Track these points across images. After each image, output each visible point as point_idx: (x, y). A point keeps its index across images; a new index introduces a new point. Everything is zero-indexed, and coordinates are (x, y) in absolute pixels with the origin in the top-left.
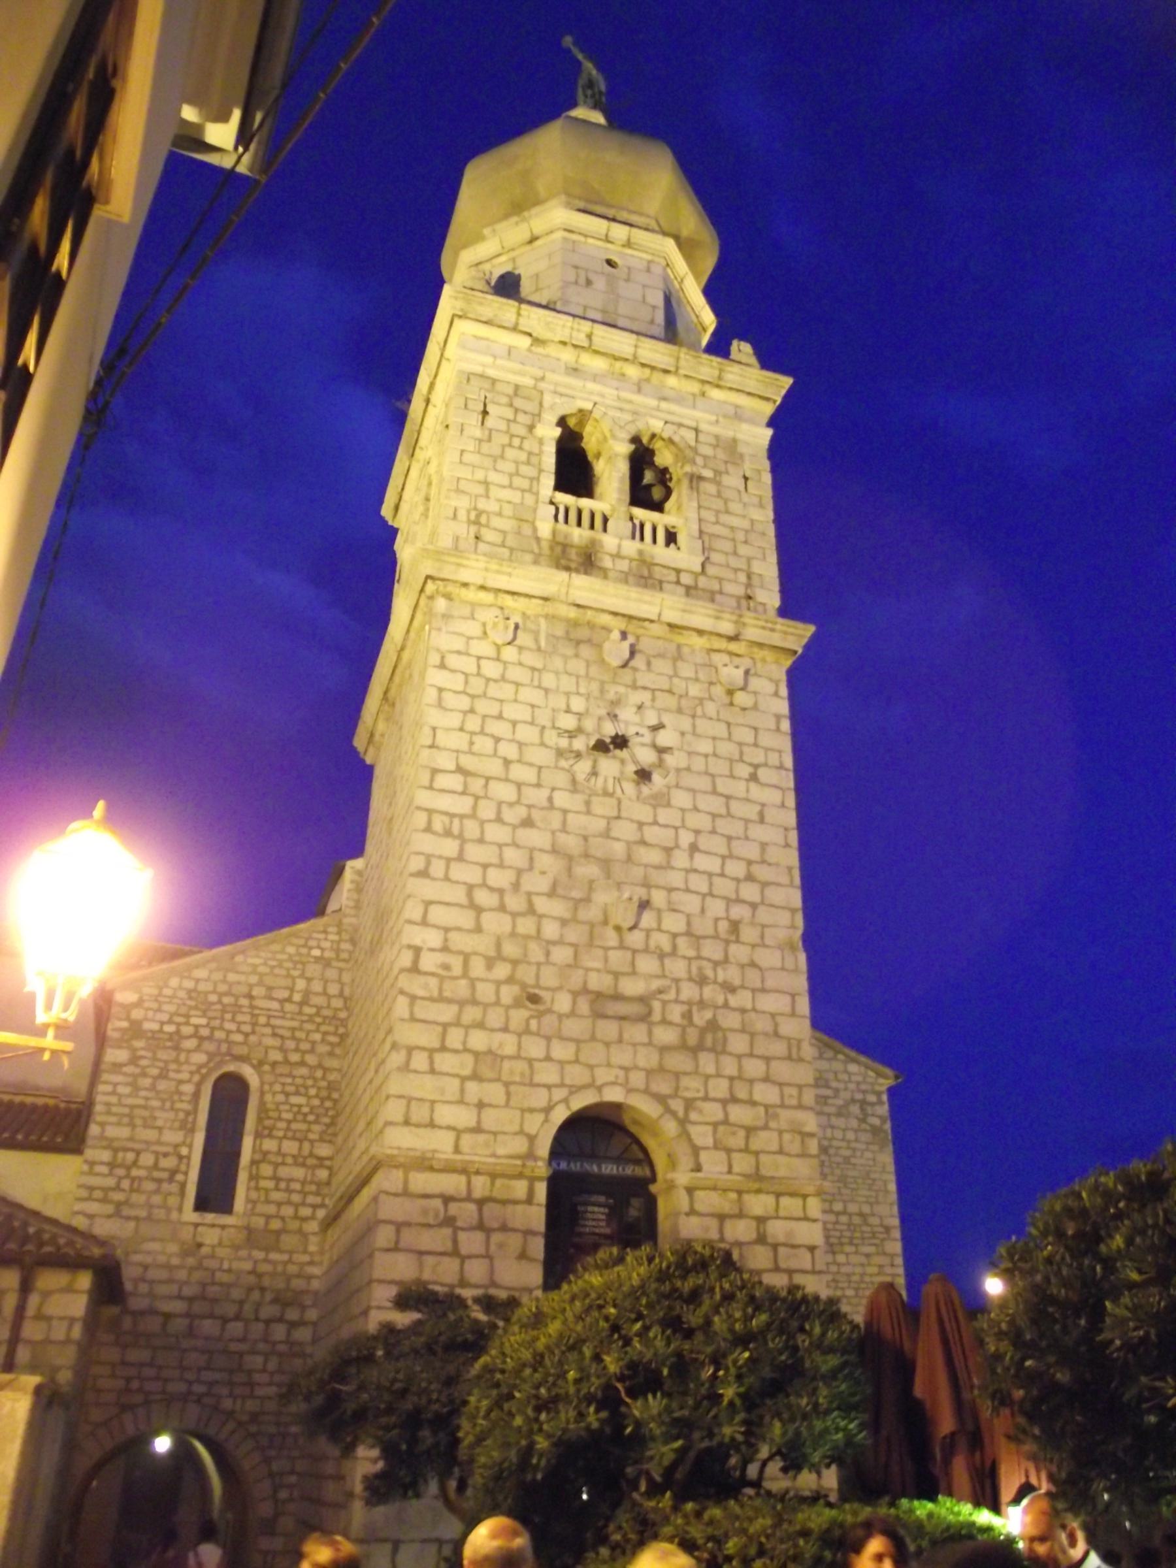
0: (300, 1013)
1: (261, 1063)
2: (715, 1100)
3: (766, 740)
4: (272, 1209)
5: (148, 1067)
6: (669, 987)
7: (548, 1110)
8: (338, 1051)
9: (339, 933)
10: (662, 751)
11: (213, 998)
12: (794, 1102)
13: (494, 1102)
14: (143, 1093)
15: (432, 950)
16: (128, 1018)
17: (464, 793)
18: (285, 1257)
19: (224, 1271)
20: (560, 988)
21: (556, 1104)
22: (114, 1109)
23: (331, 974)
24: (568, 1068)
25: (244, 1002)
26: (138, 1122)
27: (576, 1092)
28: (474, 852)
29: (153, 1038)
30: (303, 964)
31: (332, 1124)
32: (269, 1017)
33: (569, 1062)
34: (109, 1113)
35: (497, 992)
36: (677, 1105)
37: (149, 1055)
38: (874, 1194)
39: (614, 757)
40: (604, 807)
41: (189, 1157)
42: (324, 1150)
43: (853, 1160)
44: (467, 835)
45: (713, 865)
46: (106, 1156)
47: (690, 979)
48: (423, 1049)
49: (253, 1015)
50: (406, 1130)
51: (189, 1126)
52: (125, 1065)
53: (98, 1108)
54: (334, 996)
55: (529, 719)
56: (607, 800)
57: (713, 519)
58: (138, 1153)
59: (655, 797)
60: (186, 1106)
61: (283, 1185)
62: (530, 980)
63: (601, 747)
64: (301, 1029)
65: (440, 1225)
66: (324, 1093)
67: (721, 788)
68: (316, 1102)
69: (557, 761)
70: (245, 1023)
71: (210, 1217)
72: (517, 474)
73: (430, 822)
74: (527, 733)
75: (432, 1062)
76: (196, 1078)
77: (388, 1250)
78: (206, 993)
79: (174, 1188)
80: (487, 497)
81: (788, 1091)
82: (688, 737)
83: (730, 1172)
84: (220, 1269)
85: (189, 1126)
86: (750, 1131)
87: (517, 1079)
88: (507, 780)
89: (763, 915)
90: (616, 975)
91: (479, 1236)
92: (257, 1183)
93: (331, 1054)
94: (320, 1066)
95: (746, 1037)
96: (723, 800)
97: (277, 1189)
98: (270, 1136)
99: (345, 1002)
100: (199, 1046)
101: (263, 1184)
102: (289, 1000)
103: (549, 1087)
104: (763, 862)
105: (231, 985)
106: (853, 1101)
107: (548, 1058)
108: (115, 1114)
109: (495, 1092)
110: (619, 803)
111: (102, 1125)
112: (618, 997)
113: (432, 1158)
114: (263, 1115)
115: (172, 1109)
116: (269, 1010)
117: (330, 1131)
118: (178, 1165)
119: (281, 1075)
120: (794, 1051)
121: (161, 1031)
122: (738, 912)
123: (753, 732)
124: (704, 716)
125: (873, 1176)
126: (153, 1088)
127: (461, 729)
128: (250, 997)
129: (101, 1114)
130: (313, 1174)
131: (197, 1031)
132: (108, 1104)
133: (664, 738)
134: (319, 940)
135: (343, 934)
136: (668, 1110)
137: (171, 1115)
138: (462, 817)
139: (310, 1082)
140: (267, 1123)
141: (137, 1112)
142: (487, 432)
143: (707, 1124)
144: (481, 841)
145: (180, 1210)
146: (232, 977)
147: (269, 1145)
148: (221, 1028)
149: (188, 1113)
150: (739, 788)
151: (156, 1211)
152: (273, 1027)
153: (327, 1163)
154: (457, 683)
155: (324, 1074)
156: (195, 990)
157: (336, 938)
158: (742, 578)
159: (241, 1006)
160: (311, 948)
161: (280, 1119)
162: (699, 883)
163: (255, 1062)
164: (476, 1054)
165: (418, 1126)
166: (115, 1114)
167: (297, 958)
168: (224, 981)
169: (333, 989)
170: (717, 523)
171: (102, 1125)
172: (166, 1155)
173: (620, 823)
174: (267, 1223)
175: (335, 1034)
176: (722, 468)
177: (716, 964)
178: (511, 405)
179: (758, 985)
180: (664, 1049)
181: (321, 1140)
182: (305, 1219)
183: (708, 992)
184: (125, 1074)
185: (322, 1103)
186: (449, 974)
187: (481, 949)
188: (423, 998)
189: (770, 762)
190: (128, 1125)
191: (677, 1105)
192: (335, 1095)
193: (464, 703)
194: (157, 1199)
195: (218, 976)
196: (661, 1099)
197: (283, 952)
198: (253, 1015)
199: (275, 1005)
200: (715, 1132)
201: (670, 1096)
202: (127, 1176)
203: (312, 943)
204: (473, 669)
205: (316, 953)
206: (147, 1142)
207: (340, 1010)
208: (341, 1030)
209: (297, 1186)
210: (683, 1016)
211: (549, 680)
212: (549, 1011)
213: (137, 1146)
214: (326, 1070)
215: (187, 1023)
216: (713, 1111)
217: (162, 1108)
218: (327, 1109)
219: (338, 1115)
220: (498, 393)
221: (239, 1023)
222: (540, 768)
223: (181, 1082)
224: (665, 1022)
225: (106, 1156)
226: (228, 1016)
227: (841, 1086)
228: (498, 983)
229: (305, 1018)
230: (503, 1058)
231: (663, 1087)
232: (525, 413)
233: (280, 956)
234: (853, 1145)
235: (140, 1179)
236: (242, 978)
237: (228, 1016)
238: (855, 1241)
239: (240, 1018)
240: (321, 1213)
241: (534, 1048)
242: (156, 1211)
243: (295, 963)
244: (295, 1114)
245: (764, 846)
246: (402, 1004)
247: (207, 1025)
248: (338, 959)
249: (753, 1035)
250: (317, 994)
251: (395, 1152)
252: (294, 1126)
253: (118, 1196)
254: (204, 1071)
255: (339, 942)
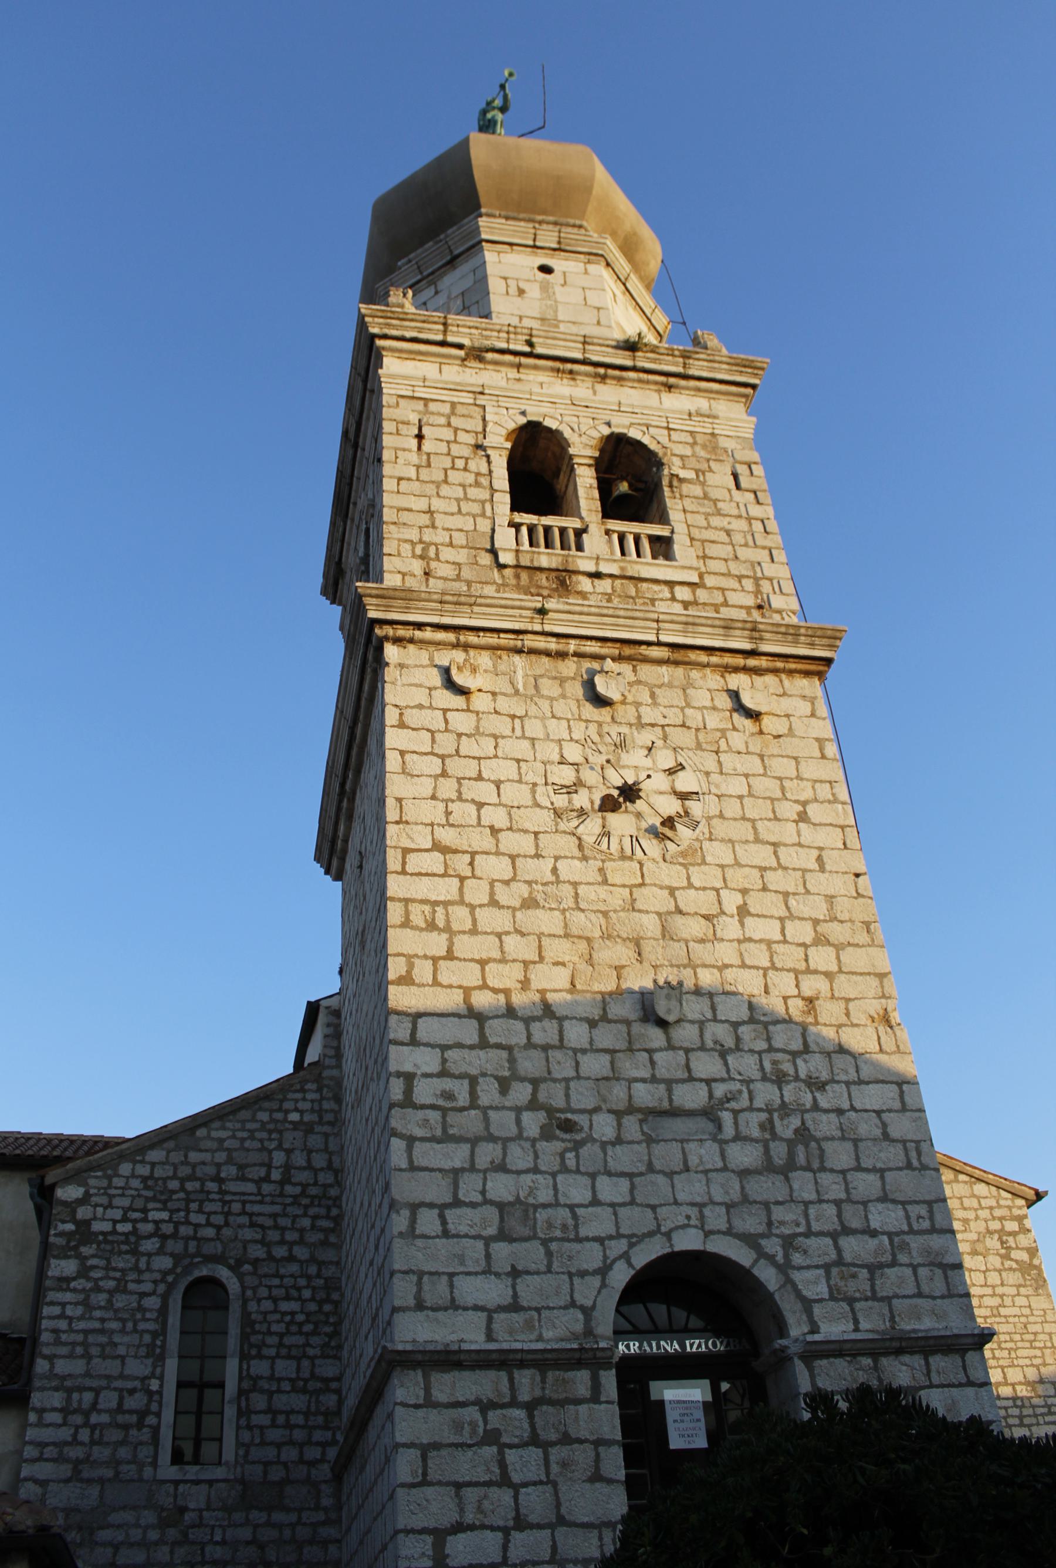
0: (282, 1195)
1: (239, 1263)
2: (820, 1234)
3: (812, 770)
4: (271, 1453)
5: (101, 1279)
6: (740, 1092)
7: (604, 1271)
8: (333, 1239)
9: (319, 1090)
10: (683, 796)
11: (174, 1185)
12: (926, 1224)
13: (533, 1267)
14: (98, 1314)
15: (426, 1075)
16: (74, 1220)
17: (445, 875)
18: (293, 1517)
19: (217, 1543)
20: (596, 1110)
21: (614, 1261)
22: (64, 1337)
23: (315, 1141)
24: (623, 1212)
25: (212, 1186)
26: (94, 1351)
27: (638, 1242)
28: (465, 946)
29: (106, 1241)
30: (280, 1132)
31: (336, 1333)
32: (244, 1203)
33: (623, 1205)
34: (58, 1342)
35: (518, 1122)
36: (773, 1246)
37: (102, 1263)
38: (1038, 1353)
39: (626, 811)
40: (623, 873)
41: (160, 1393)
42: (328, 1369)
43: (1003, 1311)
44: (455, 926)
45: (770, 930)
46: (57, 1399)
47: (764, 1078)
48: (431, 1205)
49: (225, 1203)
50: (421, 1315)
51: (158, 1351)
52: (74, 1279)
53: (45, 1337)
54: (322, 1169)
55: (516, 778)
56: (627, 864)
57: (704, 524)
58: (97, 1392)
59: (683, 854)
60: (151, 1326)
61: (281, 1419)
62: (559, 1102)
63: (609, 805)
64: (285, 1215)
65: (480, 1444)
66: (321, 1295)
67: (764, 835)
68: (312, 1307)
69: (557, 824)
70: (215, 1213)
71: (192, 1472)
72: (466, 498)
73: (407, 913)
74: (513, 793)
75: (444, 1222)
76: (162, 1288)
77: (413, 1485)
78: (165, 1180)
79: (145, 1435)
80: (433, 526)
81: (914, 1210)
82: (714, 777)
83: (856, 1330)
84: (211, 1541)
85: (158, 1351)
86: (874, 1269)
87: (558, 1233)
88: (498, 853)
89: (845, 986)
90: (669, 1083)
91: (534, 1454)
92: (249, 1419)
93: (325, 1243)
94: (313, 1259)
95: (849, 1146)
96: (770, 848)
97: (274, 1425)
98: (260, 1356)
99: (336, 1177)
100: (162, 1246)
101: (257, 1420)
102: (267, 1179)
103: (600, 1240)
104: (834, 919)
105: (194, 1166)
106: (990, 1232)
107: (595, 1202)
108: (65, 1344)
109: (532, 1254)
110: (641, 865)
111: (51, 1358)
112: (675, 1112)
113: (460, 1351)
114: (248, 1330)
115: (135, 1330)
116: (244, 1194)
117: (333, 1344)
118: (148, 1404)
119: (266, 1276)
120: (913, 1154)
121: (114, 1232)
122: (811, 985)
123: (793, 762)
124: (730, 750)
125: (1032, 1328)
126: (109, 1305)
127: (433, 797)
128: (218, 1179)
129: (48, 1344)
130: (318, 1402)
131: (158, 1229)
132: (56, 1331)
133: (686, 782)
134: (296, 1101)
135: (325, 1090)
136: (762, 1254)
137: (135, 1339)
138: (446, 904)
139: (302, 1282)
140: (254, 1339)
141: (91, 1339)
142: (425, 457)
143: (817, 1267)
144: (474, 931)
145: (154, 1464)
146: (194, 1156)
147: (259, 1367)
148: (188, 1222)
149: (155, 1334)
150: (788, 832)
151: (124, 1468)
152: (251, 1215)
153: (334, 1385)
154: (423, 741)
155: (319, 1270)
156: (151, 1176)
157: (316, 1096)
158: (749, 585)
159: (209, 1192)
160: (287, 1112)
161: (269, 1333)
162: (759, 956)
163: (232, 1262)
164: (501, 1207)
165: (434, 1309)
166: (65, 1344)
167: (271, 1126)
168: (185, 1163)
169: (319, 1161)
170: (708, 527)
171: (51, 1358)
172: (132, 1392)
173: (645, 890)
174: (265, 1473)
175: (328, 1217)
176: (704, 466)
177: (795, 1054)
178: (449, 425)
179: (852, 1076)
180: (744, 1173)
181: (323, 1356)
182: (312, 1464)
183: (789, 1092)
184: (75, 1290)
185: (321, 1307)
186: (454, 1104)
187: (490, 1069)
188: (423, 1139)
189: (820, 797)
190: (82, 1356)
191: (773, 1246)
192: (335, 1296)
193: (434, 765)
194: (123, 1452)
195: (176, 1157)
196: (750, 1240)
197: (253, 1119)
198: (225, 1203)
199: (251, 1187)
200: (828, 1277)
201: (763, 1236)
202: (86, 1424)
203: (287, 1105)
204: (439, 724)
205: (294, 1117)
206: (108, 1377)
207: (331, 1186)
208: (335, 1212)
209: (300, 1420)
210: (762, 1126)
211: (534, 728)
212: (590, 1139)
213: (95, 1383)
214: (321, 1264)
215: (145, 1220)
216: (821, 1248)
217: (123, 1331)
218: (327, 1315)
219: (339, 1323)
220: (432, 413)
221: (209, 1214)
222: (536, 834)
223: (143, 1295)
224: (738, 1137)
225: (57, 1399)
226: (194, 1206)
227: (971, 1215)
228: (518, 1110)
229: (289, 1200)
230: (536, 1207)
231: (751, 1222)
232: (467, 431)
233: (249, 1126)
234: (999, 1290)
235: (102, 1426)
236: (207, 1157)
237: (194, 1206)
238: (1026, 1421)
239: (209, 1207)
240: (332, 1453)
241: (576, 1190)
242: (124, 1468)
243: (270, 1132)
244: (288, 1324)
245: (830, 899)
246: (397, 1145)
247: (170, 1220)
248: (321, 1122)
249: (856, 1142)
250: (299, 1168)
251: (409, 1347)
252: (287, 1341)
253: (75, 1453)
254: (170, 1279)
255: (320, 1101)
